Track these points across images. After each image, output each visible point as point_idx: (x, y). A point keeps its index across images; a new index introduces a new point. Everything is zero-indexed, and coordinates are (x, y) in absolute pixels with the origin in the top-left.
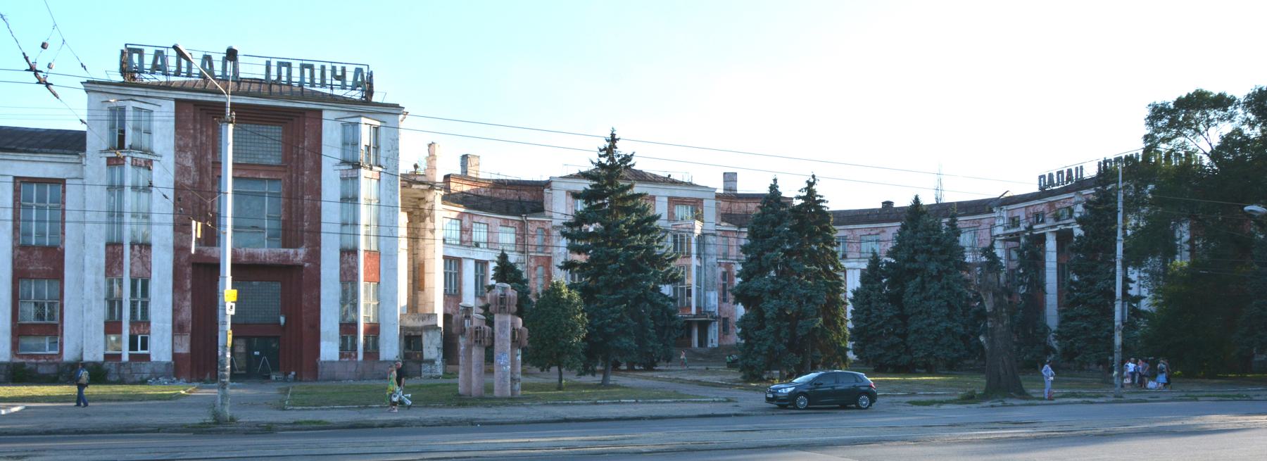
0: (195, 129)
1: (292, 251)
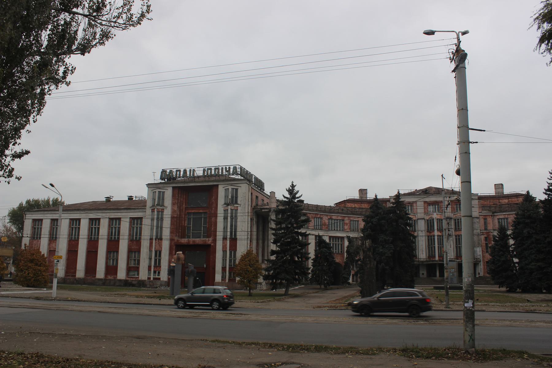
0: (178, 196)
1: (207, 239)
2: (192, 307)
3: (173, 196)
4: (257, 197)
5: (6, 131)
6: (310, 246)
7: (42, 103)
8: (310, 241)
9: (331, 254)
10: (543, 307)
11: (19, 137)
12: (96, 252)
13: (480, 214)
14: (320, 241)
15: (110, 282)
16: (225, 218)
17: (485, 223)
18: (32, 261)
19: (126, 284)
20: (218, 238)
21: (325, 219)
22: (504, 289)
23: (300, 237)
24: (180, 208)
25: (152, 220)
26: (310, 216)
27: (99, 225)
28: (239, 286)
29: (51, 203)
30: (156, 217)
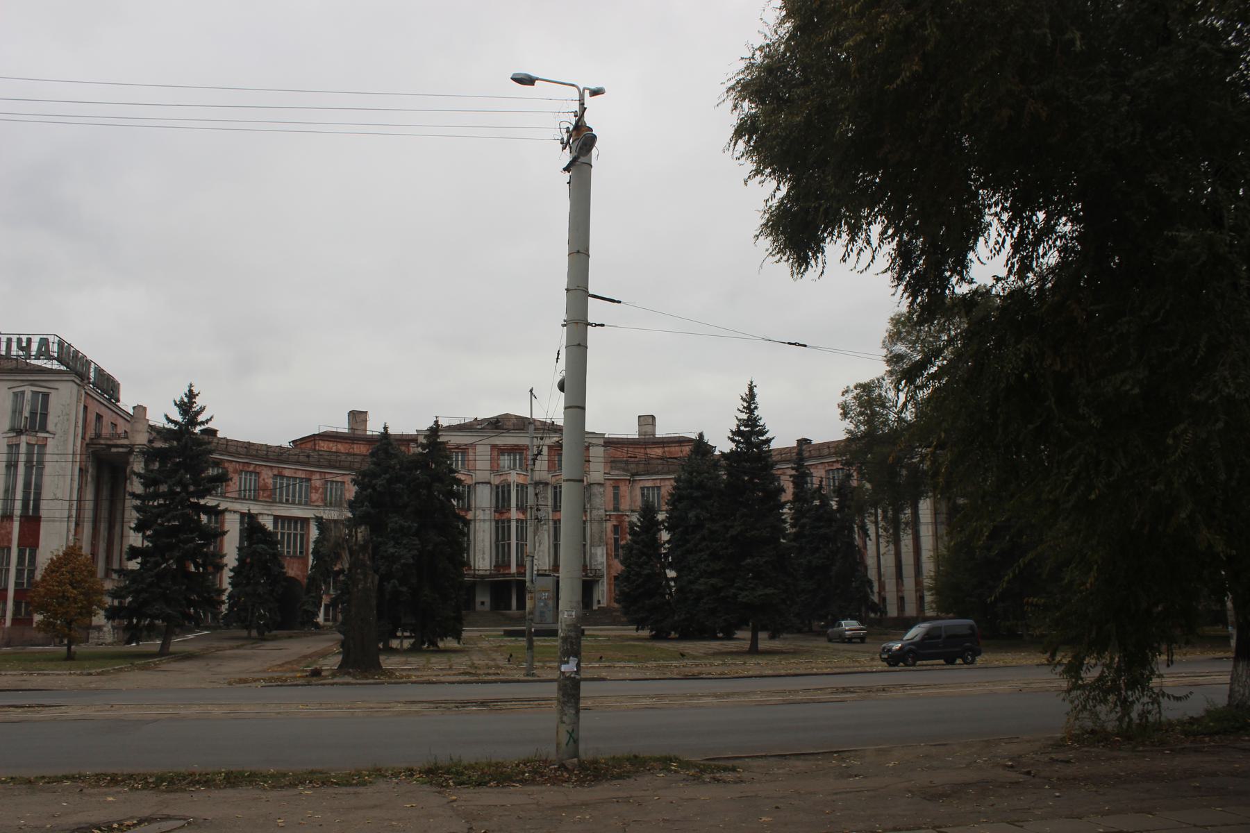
6: (227, 538)
8: (227, 527)
9: (276, 557)
10: (716, 666)
13: (608, 477)
14: (251, 527)
17: (616, 497)
21: (267, 476)
22: (646, 633)
23: (204, 518)
26: (230, 467)
28: (41, 635)
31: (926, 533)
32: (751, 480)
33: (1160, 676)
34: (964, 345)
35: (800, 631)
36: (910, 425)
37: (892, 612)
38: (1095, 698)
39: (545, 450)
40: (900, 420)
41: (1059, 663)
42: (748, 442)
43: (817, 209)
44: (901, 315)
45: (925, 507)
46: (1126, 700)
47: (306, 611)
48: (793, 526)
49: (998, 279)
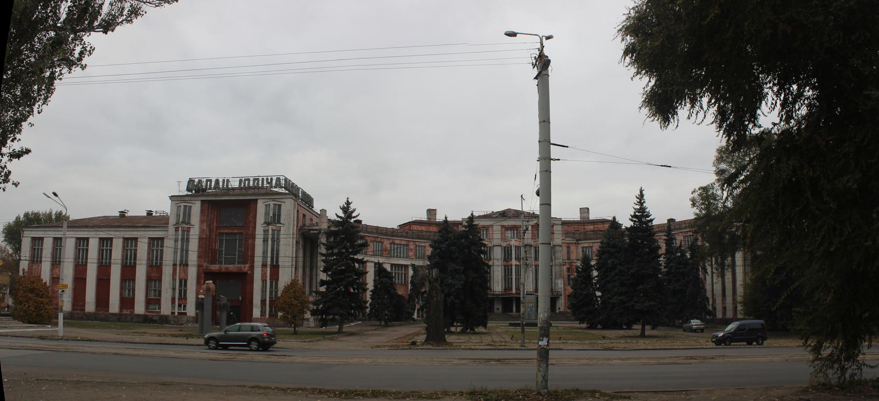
2: (225, 348)
3: (202, 211)
4: (304, 216)
5: (5, 123)
6: (368, 275)
7: (50, 90)
8: (368, 270)
9: (392, 285)
10: (622, 344)
11: (20, 131)
12: (109, 280)
14: (380, 270)
15: (126, 317)
16: (265, 240)
17: (568, 252)
18: (32, 291)
19: (146, 320)
20: (256, 264)
21: (387, 244)
22: (584, 325)
23: (357, 265)
24: (210, 227)
25: (176, 240)
26: (369, 239)
27: (111, 246)
28: (282, 322)
29: (54, 217)
30: (180, 237)
31: (739, 271)
32: (642, 242)
33: (864, 354)
34: (758, 163)
35: (668, 325)
36: (730, 210)
37: (719, 315)
38: (827, 366)
39: (530, 228)
40: (725, 207)
41: (809, 345)
42: (640, 221)
43: (672, 91)
44: (722, 147)
45: (739, 256)
46: (844, 367)
47: (408, 312)
48: (665, 267)
49: (775, 124)
